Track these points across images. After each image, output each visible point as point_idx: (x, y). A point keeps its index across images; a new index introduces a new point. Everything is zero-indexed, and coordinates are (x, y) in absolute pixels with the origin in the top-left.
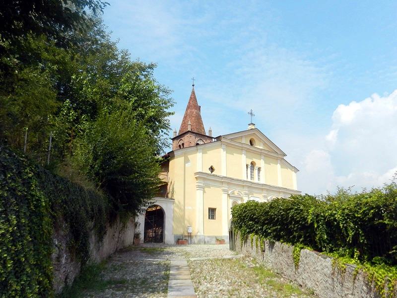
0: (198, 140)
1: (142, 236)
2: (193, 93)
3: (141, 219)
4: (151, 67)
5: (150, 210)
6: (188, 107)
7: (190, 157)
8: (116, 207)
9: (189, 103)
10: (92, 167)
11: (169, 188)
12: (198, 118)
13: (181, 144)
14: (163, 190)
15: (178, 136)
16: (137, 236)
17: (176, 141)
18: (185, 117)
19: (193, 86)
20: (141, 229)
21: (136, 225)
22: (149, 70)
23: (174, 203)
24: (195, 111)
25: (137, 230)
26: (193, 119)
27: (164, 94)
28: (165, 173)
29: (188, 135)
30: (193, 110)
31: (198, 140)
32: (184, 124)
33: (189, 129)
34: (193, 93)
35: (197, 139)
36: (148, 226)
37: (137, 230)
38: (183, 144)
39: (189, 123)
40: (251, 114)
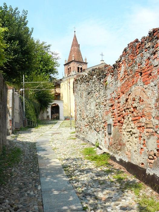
0: (79, 65)
1: (50, 117)
2: (75, 36)
3: (49, 110)
4: (49, 46)
5: (54, 105)
6: (72, 46)
7: (39, 125)
8: (42, 106)
9: (73, 43)
10: (34, 95)
11: (61, 95)
12: (79, 52)
13: (69, 68)
14: (58, 96)
15: (67, 63)
16: (48, 117)
17: (66, 66)
18: (71, 52)
19: (75, 32)
20: (50, 114)
21: (47, 112)
22: (48, 47)
23: (63, 102)
24: (76, 48)
25: (48, 114)
26: (75, 52)
27: (55, 55)
28: (59, 89)
29: (73, 63)
30: (75, 47)
31: (79, 65)
32: (70, 56)
33: (73, 59)
34: (75, 36)
35: (78, 65)
36: (52, 113)
37: (48, 114)
38: (70, 68)
39: (73, 56)
40: (102, 55)
